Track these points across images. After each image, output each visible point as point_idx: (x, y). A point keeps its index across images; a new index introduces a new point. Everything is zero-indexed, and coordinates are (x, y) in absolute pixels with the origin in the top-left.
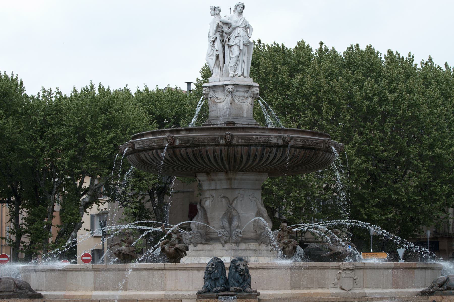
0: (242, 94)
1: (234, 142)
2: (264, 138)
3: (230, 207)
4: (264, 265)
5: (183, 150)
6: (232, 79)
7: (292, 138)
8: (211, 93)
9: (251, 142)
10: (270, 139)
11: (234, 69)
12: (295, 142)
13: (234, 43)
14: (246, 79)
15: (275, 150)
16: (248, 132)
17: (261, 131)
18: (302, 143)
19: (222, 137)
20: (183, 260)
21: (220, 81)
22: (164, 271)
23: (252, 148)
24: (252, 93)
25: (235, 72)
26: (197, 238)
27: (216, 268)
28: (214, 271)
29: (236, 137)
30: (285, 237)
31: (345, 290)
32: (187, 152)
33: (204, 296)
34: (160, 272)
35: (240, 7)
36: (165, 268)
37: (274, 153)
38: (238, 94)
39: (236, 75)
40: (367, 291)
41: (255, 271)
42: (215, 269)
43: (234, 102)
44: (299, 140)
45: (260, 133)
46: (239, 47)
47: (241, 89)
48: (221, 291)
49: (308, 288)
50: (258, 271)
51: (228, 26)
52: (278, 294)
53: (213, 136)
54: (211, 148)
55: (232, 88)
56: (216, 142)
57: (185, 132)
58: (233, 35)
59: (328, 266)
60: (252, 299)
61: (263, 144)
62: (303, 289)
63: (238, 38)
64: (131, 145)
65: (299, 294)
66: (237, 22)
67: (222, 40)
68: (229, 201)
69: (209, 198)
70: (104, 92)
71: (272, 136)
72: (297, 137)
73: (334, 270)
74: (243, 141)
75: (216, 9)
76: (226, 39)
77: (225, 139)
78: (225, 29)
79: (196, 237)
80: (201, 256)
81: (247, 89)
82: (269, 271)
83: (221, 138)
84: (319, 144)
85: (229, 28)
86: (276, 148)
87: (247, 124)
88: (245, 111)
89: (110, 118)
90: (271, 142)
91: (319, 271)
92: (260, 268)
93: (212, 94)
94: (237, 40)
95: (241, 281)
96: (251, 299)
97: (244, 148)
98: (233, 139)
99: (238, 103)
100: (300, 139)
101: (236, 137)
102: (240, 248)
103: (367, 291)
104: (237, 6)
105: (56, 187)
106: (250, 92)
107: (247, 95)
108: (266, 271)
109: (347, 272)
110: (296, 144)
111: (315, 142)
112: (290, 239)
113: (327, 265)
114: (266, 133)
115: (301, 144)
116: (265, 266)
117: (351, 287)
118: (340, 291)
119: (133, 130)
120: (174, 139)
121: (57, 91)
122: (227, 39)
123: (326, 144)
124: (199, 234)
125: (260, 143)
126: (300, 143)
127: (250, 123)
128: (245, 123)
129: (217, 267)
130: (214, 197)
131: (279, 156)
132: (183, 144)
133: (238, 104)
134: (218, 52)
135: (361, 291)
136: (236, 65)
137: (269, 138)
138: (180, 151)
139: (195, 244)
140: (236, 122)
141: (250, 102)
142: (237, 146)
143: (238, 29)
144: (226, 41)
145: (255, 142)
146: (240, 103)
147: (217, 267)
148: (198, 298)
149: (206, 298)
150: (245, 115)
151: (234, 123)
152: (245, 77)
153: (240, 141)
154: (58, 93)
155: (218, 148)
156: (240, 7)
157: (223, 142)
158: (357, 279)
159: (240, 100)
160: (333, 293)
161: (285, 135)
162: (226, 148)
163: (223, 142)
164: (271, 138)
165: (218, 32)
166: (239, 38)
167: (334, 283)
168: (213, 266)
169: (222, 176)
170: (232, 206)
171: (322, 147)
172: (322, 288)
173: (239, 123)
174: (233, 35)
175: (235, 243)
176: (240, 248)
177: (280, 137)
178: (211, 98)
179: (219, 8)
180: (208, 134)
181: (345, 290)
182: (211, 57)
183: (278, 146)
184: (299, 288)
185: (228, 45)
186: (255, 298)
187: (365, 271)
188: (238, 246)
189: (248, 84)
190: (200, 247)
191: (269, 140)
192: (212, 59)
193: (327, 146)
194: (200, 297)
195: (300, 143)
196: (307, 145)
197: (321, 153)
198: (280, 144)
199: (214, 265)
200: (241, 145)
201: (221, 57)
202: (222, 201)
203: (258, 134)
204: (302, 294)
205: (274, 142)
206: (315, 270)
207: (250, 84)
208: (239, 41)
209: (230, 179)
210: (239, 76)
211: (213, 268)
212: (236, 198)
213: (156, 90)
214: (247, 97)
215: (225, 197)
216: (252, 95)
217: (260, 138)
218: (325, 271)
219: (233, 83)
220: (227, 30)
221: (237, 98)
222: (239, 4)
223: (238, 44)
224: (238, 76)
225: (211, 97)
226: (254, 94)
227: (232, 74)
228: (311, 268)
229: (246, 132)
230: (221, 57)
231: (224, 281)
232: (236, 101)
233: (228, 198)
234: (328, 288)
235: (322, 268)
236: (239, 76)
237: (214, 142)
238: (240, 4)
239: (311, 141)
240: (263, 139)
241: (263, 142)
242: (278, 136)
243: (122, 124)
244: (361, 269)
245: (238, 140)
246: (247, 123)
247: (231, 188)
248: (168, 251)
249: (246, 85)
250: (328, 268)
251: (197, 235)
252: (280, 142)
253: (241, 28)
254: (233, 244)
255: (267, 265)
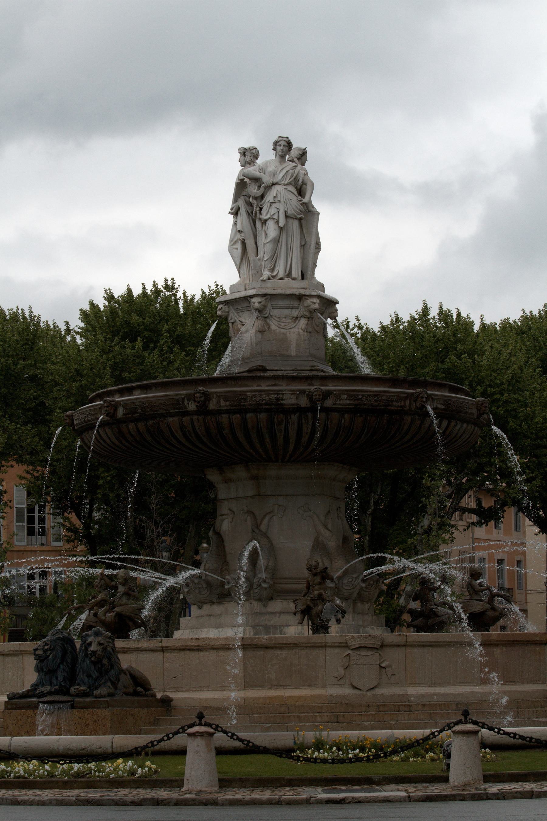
0: (287, 312)
1: (212, 405)
2: (268, 395)
3: (256, 530)
4: (189, 643)
5: (131, 426)
6: (264, 285)
7: (327, 394)
8: (231, 315)
9: (244, 405)
10: (280, 397)
11: (269, 265)
12: (336, 401)
13: (268, 216)
14: (294, 284)
15: (294, 418)
16: (247, 386)
17: (271, 382)
18: (352, 402)
19: (190, 397)
20: (177, 634)
21: (246, 290)
22: (21, 657)
23: (249, 415)
24: (306, 309)
25: (272, 270)
26: (200, 592)
27: (52, 650)
28: (49, 656)
29: (215, 396)
30: (317, 587)
31: (360, 690)
32: (138, 430)
33: (16, 704)
34: (16, 658)
35: (280, 145)
36: (21, 651)
37: (296, 424)
38: (276, 312)
39: (274, 277)
40: (411, 691)
41: (176, 654)
42: (49, 652)
43: (269, 328)
44: (346, 396)
45: (269, 386)
46: (278, 222)
47: (281, 303)
48: (50, 693)
49: (279, 686)
50: (182, 654)
51: (257, 184)
52: (217, 699)
53: (174, 397)
54: (176, 419)
55: (259, 303)
56: (180, 408)
57: (139, 391)
58: (267, 201)
59: (321, 643)
60: (100, 709)
61: (267, 407)
62: (271, 688)
63: (274, 206)
64: (67, 421)
65: (259, 698)
66: (274, 175)
67: (250, 212)
68: (255, 519)
69: (227, 515)
70: (35, 321)
71: (285, 390)
72: (339, 390)
73: (337, 651)
74: (228, 403)
75: (247, 153)
76: (256, 209)
77: (195, 401)
78: (253, 190)
79: (197, 591)
80: (204, 627)
81: (296, 303)
82: (202, 654)
83: (189, 400)
84: (397, 402)
85: (259, 187)
86: (297, 414)
87: (292, 370)
88: (293, 346)
89: (449, 369)
90: (284, 402)
91: (304, 652)
92: (184, 649)
93: (233, 316)
94: (273, 210)
95: (95, 674)
96: (98, 710)
97: (233, 417)
98: (209, 401)
99: (278, 330)
100: (347, 395)
101: (215, 396)
102: (269, 609)
103: (411, 691)
104: (276, 143)
105: (374, 502)
106: (301, 307)
107: (295, 313)
108: (195, 654)
109: (363, 653)
110: (340, 404)
111: (384, 397)
112: (321, 591)
113: (319, 641)
114: (281, 385)
115: (351, 404)
116: (193, 644)
117: (374, 684)
118: (348, 691)
119: (489, 389)
120: (115, 406)
121: (357, 324)
122: (258, 209)
123: (415, 401)
124: (204, 585)
125: (261, 405)
126: (348, 402)
127: (299, 368)
128: (288, 368)
129: (53, 649)
130: (234, 512)
131: (307, 429)
132: (129, 414)
133: (278, 331)
134: (242, 235)
135: (398, 691)
136: (274, 257)
137: (278, 395)
138: (127, 427)
139: (200, 605)
140: (268, 368)
141: (304, 327)
142: (220, 412)
143: (276, 188)
144: (256, 213)
145: (250, 405)
146: (282, 330)
147: (53, 649)
148: (6, 708)
149: (21, 708)
150: (293, 353)
151: (264, 370)
152: (294, 279)
153: (222, 403)
154: (360, 327)
155: (186, 419)
156: (280, 145)
157: (192, 406)
158: (390, 666)
159: (283, 324)
160: (331, 695)
161: (313, 388)
162: (201, 418)
163: (192, 406)
164: (283, 394)
165: (242, 197)
166: (277, 205)
167: (335, 675)
168: (46, 647)
169: (240, 472)
170: (260, 531)
171: (405, 406)
172: (310, 686)
173: (276, 368)
174: (267, 201)
175: (260, 600)
176: (269, 609)
177: (302, 392)
178: (233, 323)
179: (254, 151)
180: (168, 393)
181: (360, 690)
182: (235, 246)
183: (298, 409)
184: (261, 686)
185: (260, 219)
186: (105, 708)
187: (409, 650)
188: (265, 606)
189: (294, 293)
190: (207, 608)
191: (278, 399)
192: (237, 249)
193: (418, 404)
194: (9, 706)
195: (348, 402)
196: (365, 404)
197: (408, 419)
198: (303, 406)
199: (48, 645)
200: (228, 412)
201: (250, 243)
202: (246, 521)
203: (264, 387)
204: (265, 698)
205: (290, 401)
206: (294, 651)
207: (297, 293)
208: (276, 211)
209: (255, 478)
210: (281, 279)
211: (46, 651)
212: (270, 513)
213: (439, 314)
214: (297, 318)
215: (250, 513)
216: (308, 314)
217: (260, 395)
218: (315, 652)
219: (260, 293)
220: (255, 191)
221: (274, 321)
222: (279, 139)
223: (276, 217)
224: (279, 277)
225: (232, 321)
226: (310, 312)
227: (266, 274)
228: (286, 647)
229: (241, 386)
230: (250, 243)
231: (66, 674)
232: (273, 327)
233: (254, 514)
234: (324, 686)
235: (310, 647)
236: (281, 279)
237: (177, 409)
238: (281, 139)
239: (375, 396)
240: (267, 398)
241: (267, 404)
242: (298, 390)
243: (470, 379)
244: (399, 646)
245: (219, 402)
246: (294, 368)
247: (259, 495)
248: (103, 618)
249: (290, 295)
250: (322, 647)
251: (200, 586)
252: (304, 402)
253: (281, 186)
254: (255, 603)
255: (195, 643)
